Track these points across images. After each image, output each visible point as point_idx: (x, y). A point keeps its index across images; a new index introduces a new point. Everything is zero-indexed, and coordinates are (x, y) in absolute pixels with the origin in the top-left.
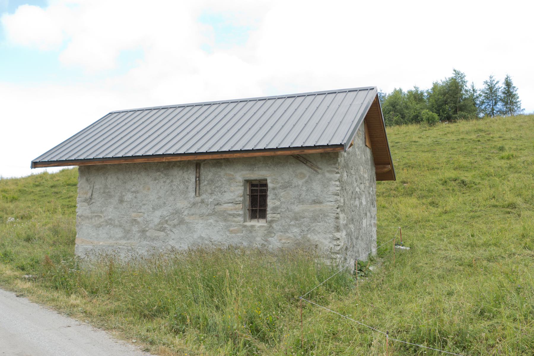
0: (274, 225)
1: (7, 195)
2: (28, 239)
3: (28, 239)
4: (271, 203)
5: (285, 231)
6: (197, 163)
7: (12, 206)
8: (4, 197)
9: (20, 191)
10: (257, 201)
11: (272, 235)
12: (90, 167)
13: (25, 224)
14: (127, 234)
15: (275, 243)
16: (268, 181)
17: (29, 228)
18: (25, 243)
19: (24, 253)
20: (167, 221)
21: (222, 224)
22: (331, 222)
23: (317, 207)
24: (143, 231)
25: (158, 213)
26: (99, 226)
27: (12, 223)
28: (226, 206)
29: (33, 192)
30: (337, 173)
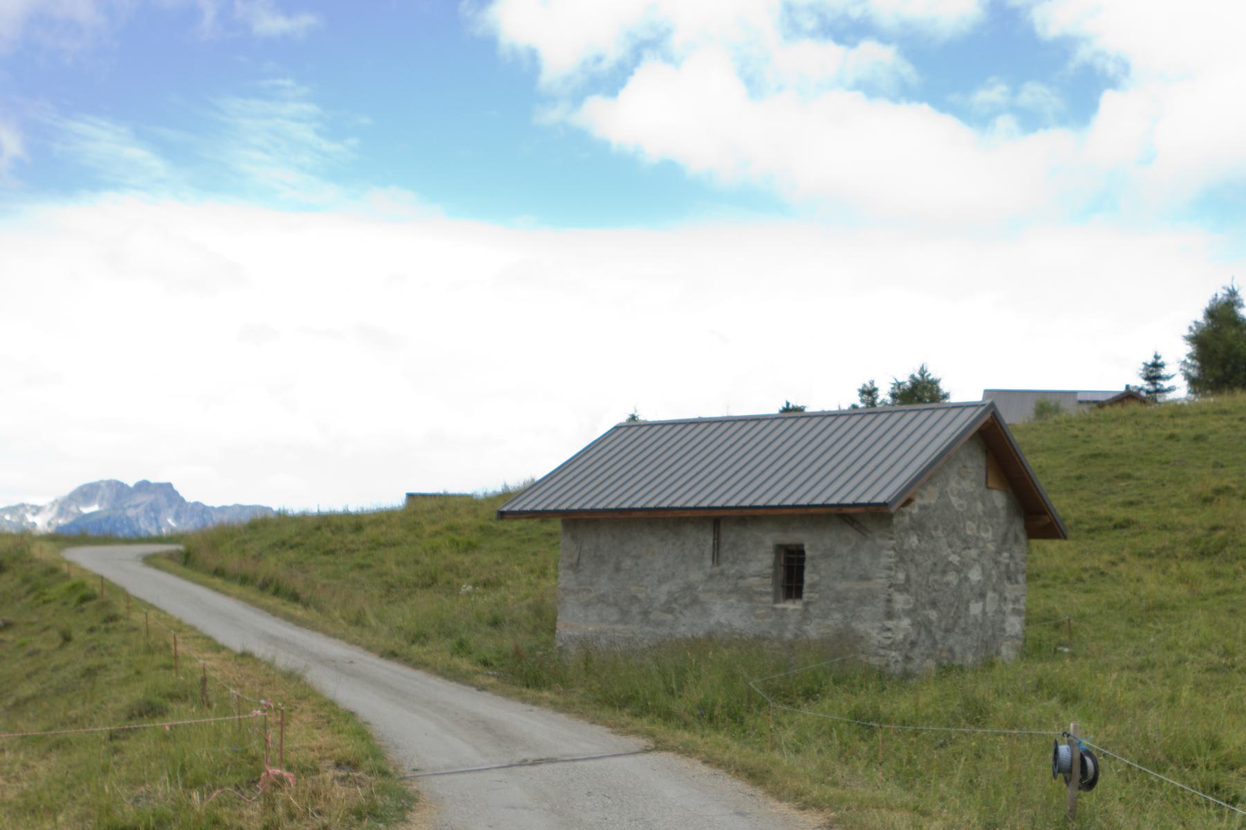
0: (811, 609)
1: (457, 538)
2: (495, 623)
3: (495, 623)
4: (809, 577)
5: (825, 616)
6: (718, 522)
7: (466, 560)
8: (452, 541)
9: (482, 528)
10: (791, 575)
11: (807, 621)
12: (578, 521)
13: (492, 597)
14: (624, 617)
15: (813, 631)
16: (806, 548)
17: (496, 604)
18: (489, 629)
19: (487, 643)
20: (675, 600)
21: (746, 605)
22: (881, 606)
23: (865, 585)
24: (646, 613)
25: (665, 588)
26: (587, 605)
27: (468, 594)
28: (751, 580)
29: (505, 531)
30: (891, 539)
